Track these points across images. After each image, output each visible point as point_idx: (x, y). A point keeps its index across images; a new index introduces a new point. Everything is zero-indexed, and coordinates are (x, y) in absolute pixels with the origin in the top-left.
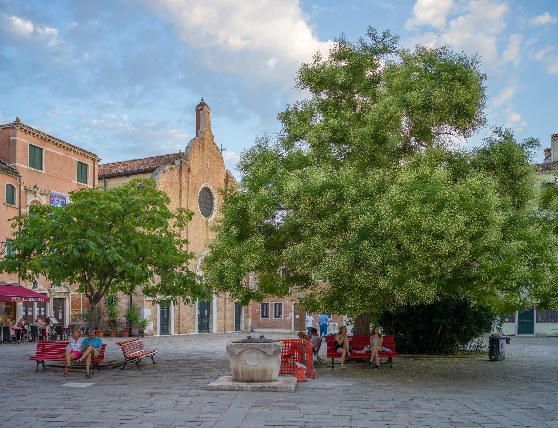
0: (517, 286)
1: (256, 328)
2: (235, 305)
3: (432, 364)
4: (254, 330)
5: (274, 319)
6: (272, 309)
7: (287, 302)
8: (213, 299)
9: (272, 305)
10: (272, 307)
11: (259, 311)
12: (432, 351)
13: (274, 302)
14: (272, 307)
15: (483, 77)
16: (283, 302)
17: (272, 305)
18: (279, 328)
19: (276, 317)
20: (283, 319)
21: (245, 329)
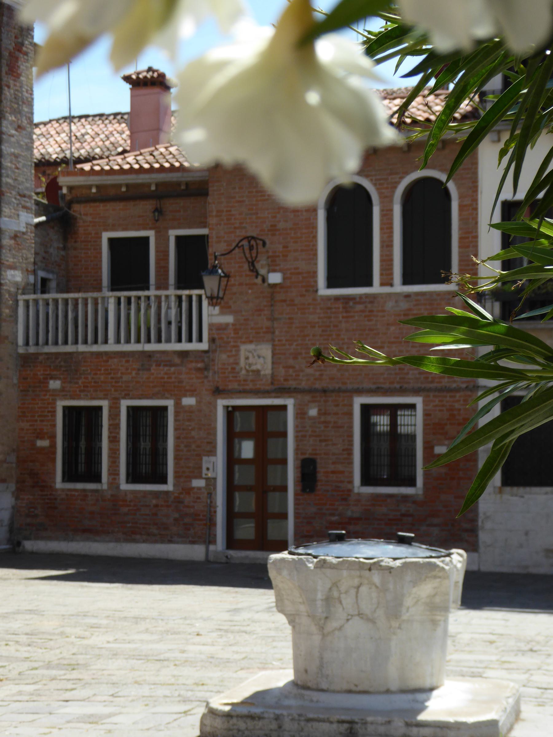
0: (45, 379)
4: (29, 545)
5: (125, 486)
6: (114, 439)
7: (189, 401)
8: (363, 388)
9: (114, 415)
10: (114, 427)
11: (53, 445)
12: (117, 477)
14: (114, 427)
15: (2, 259)
16: (170, 403)
17: (114, 415)
18: (151, 538)
20: (169, 487)
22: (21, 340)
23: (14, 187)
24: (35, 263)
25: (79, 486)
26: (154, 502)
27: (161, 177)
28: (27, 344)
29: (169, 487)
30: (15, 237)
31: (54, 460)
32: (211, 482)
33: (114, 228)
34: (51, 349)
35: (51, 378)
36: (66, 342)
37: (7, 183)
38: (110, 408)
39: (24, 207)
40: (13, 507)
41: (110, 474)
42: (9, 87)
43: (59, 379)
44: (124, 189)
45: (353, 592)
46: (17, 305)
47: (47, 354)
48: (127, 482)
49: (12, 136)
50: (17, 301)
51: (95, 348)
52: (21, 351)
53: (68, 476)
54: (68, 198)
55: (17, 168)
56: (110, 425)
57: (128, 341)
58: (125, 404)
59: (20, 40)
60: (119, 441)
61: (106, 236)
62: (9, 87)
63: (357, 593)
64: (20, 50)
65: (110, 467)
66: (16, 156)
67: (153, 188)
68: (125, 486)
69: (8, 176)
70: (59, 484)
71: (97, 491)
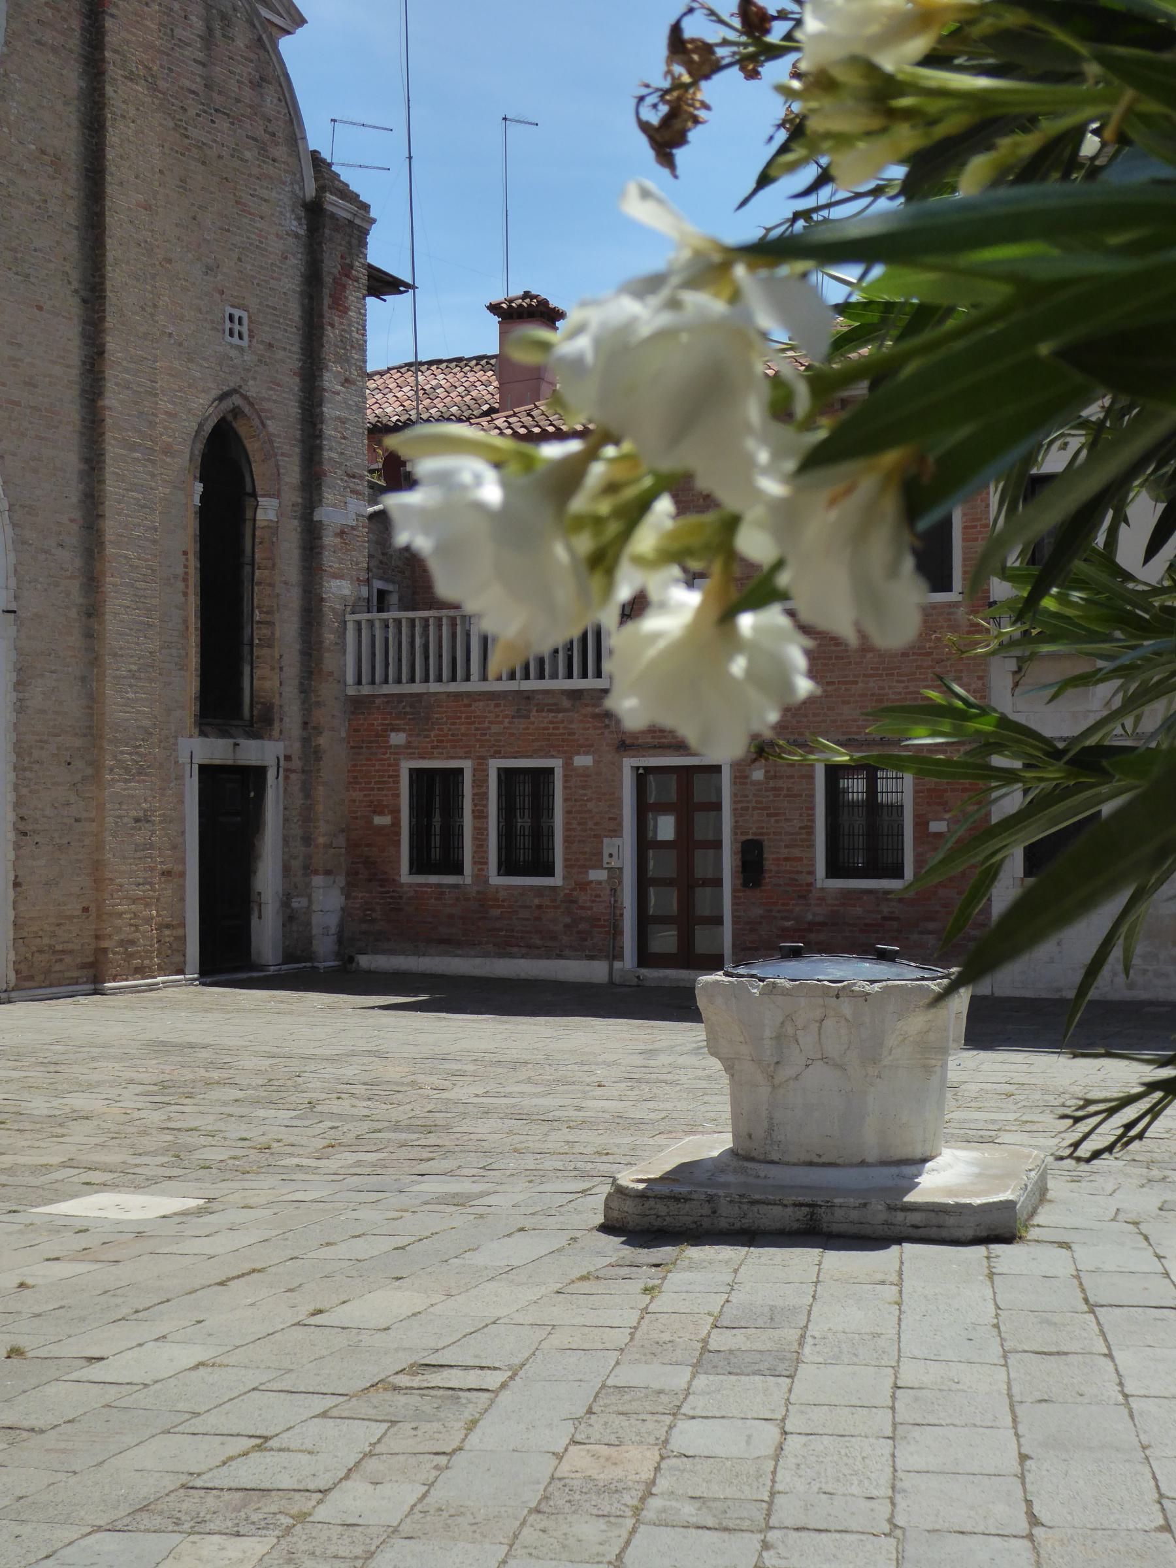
1: (376, 942)
2: (192, 788)
3: (1099, 1093)
4: (364, 961)
5: (496, 880)
6: (480, 815)
7: (583, 761)
9: (480, 781)
10: (481, 797)
11: (396, 823)
13: (494, 765)
14: (481, 797)
16: (556, 764)
17: (480, 781)
19: (508, 867)
20: (557, 880)
21: (289, 958)
22: (350, 678)
23: (341, 464)
25: (433, 879)
26: (537, 901)
29: (557, 880)
31: (397, 844)
32: (616, 874)
35: (392, 730)
37: (330, 459)
40: (342, 909)
42: (333, 326)
43: (404, 730)
46: (345, 629)
52: (351, 691)
53: (420, 865)
55: (344, 438)
58: (494, 765)
60: (486, 817)
62: (333, 326)
66: (343, 421)
69: (330, 449)
70: (405, 876)
71: (456, 886)
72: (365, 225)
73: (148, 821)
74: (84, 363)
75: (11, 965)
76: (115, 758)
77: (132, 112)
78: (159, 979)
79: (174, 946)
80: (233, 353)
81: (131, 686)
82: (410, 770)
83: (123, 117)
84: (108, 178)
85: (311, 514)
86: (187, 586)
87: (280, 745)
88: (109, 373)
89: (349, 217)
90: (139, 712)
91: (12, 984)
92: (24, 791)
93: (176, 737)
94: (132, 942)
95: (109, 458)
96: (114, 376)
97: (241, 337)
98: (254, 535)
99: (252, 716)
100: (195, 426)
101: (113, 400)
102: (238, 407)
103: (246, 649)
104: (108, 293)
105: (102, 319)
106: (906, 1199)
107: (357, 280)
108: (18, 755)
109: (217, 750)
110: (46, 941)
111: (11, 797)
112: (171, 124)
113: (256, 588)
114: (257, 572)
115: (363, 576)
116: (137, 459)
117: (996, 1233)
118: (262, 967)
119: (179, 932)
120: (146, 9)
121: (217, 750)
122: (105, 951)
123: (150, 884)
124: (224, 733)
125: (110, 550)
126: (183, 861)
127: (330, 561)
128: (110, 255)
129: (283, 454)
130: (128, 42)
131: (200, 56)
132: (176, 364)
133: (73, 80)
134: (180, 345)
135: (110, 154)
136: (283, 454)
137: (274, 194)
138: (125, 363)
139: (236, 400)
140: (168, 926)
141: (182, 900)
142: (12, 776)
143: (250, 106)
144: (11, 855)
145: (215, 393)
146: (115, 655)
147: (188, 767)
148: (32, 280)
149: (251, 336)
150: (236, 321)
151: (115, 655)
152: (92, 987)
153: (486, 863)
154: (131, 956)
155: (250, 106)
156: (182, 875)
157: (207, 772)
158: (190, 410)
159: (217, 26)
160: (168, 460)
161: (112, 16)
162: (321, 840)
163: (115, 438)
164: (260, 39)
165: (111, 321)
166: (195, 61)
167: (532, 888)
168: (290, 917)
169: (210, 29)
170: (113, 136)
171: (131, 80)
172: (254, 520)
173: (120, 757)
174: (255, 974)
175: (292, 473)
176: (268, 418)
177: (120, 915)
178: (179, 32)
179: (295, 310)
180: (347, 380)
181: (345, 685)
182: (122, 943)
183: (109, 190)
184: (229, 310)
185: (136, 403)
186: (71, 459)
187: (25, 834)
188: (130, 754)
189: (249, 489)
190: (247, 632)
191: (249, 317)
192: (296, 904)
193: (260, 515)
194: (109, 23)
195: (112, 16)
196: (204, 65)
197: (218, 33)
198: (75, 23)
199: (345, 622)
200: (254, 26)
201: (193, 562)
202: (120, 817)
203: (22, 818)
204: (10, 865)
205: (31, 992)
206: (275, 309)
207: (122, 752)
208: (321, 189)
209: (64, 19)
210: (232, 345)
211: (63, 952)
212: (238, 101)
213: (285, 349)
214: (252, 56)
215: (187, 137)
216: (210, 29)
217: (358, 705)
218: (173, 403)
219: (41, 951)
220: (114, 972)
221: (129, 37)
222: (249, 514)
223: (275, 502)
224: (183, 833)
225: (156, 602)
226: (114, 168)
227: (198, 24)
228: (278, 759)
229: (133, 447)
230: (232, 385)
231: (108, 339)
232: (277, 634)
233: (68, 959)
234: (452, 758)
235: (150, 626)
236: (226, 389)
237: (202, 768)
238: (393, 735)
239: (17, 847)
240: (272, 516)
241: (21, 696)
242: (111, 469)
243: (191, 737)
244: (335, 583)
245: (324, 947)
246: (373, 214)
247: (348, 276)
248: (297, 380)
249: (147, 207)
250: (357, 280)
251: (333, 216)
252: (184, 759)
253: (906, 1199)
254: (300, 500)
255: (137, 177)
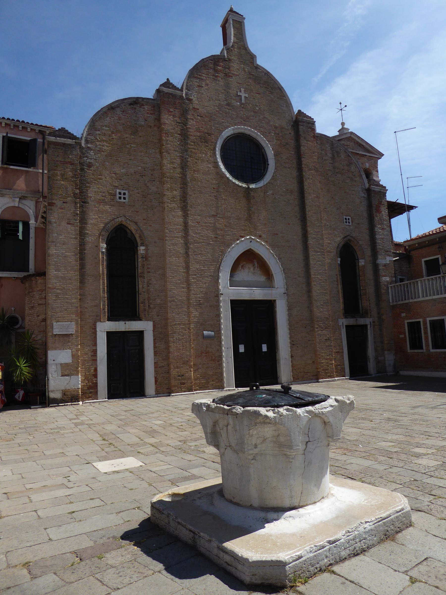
4: (402, 373)
5: (432, 351)
6: (426, 333)
11: (405, 336)
14: (426, 328)
22: (391, 301)
23: (383, 249)
24: (395, 274)
25: (416, 351)
26: (444, 356)
27: (439, 235)
28: (393, 302)
30: (385, 265)
31: (406, 342)
33: (426, 257)
34: (401, 302)
35: (402, 313)
36: (405, 300)
37: (379, 248)
38: (423, 321)
39: (388, 255)
40: (395, 359)
41: (426, 346)
42: (377, 216)
43: (405, 313)
44: (427, 243)
45: (225, 428)
46: (388, 289)
47: (400, 304)
48: (410, 349)
49: (380, 232)
50: (388, 287)
51: (415, 300)
52: (391, 304)
53: (412, 347)
54: (409, 250)
55: (384, 243)
56: (424, 328)
57: (427, 296)
58: (428, 319)
59: (380, 200)
60: (428, 334)
61: (423, 260)
62: (377, 216)
63: (227, 428)
64: (381, 204)
65: (426, 344)
66: (383, 238)
67: (438, 240)
68: (432, 351)
69: (379, 246)
70: (409, 351)
71: (422, 352)
72: (385, 191)
73: (329, 340)
74: (303, 235)
75: (292, 376)
76: (318, 325)
77: (311, 177)
78: (336, 378)
79: (342, 370)
80: (347, 227)
81: (321, 308)
82: (407, 322)
83: (309, 179)
84: (305, 193)
85: (376, 262)
86: (338, 283)
87: (371, 319)
88: (309, 236)
89: (379, 190)
90: (324, 314)
91: (292, 381)
92: (293, 335)
93: (338, 319)
94: (327, 370)
95: (310, 255)
96: (310, 237)
97: (349, 223)
98: (359, 269)
99: (362, 312)
100: (337, 245)
101: (311, 242)
102: (350, 239)
103: (359, 297)
104: (307, 218)
105: (306, 224)
106: (230, 545)
107: (384, 204)
108: (290, 326)
109: (351, 321)
110: (302, 370)
111: (289, 336)
112: (324, 178)
113: (361, 282)
114: (361, 278)
115: (393, 275)
116: (319, 255)
117: (270, 582)
118: (371, 375)
119: (342, 367)
120: (313, 154)
121: (351, 321)
122: (319, 372)
123: (331, 355)
124: (353, 317)
125: (312, 276)
126: (342, 349)
127: (382, 272)
128: (307, 210)
129: (365, 249)
130: (308, 162)
131: (331, 162)
132: (330, 231)
133: (295, 173)
134: (331, 227)
135: (305, 187)
136: (365, 249)
137: (356, 189)
138: (313, 233)
139: (349, 238)
140: (339, 365)
141: (343, 358)
142: (288, 331)
143: (347, 170)
144: (290, 350)
145: (342, 237)
146: (316, 301)
147: (342, 327)
148: (286, 218)
149: (352, 222)
150: (347, 219)
151: (316, 301)
152: (316, 381)
153: (429, 346)
154: (327, 373)
155: (347, 170)
156: (343, 352)
157: (348, 327)
158: (335, 242)
159: (335, 154)
160: (330, 254)
161: (304, 158)
162: (386, 342)
163: (312, 250)
164: (348, 155)
165: (308, 224)
166: (330, 163)
167: (442, 352)
168: (378, 362)
169: (333, 155)
170: (306, 183)
171: (310, 170)
172: (359, 265)
173: (319, 325)
174: (368, 377)
175: (368, 252)
176: (359, 241)
177: (323, 363)
178: (324, 158)
179: (365, 214)
180: (383, 229)
181: (390, 303)
182: (323, 370)
183: (306, 195)
184: (345, 217)
185: (317, 242)
186: (301, 257)
187: (294, 345)
188: (323, 324)
189: (357, 258)
190: (359, 292)
191: (351, 218)
192: (380, 358)
193: (360, 264)
194: (303, 159)
195: (304, 158)
196: (332, 164)
197: (336, 156)
198: (295, 161)
199: (388, 287)
200: (346, 152)
201: (339, 278)
202: (321, 339)
203: (293, 341)
204: (290, 352)
205: (298, 382)
206: (359, 215)
207: (320, 324)
208: (370, 185)
209: (291, 161)
210: (346, 225)
211: (307, 372)
212: (343, 170)
213: (363, 224)
214: (346, 159)
215: (329, 180)
216: (333, 155)
217: (393, 307)
218: (330, 241)
219: (300, 372)
220: (322, 377)
221: (309, 161)
222: (357, 264)
223: (363, 260)
224: (342, 342)
225: (327, 287)
226: (306, 190)
227: (330, 155)
228: (370, 322)
229: (317, 252)
230: (347, 234)
231: (308, 228)
232: (367, 292)
233: (308, 374)
234: (417, 319)
235: (327, 293)
236: (346, 235)
237: (346, 326)
238: (402, 314)
239: (291, 348)
240: (363, 264)
241: (290, 312)
242: (311, 258)
243: (342, 319)
244: (384, 278)
245: (390, 370)
246: (387, 189)
247: (381, 204)
248: (368, 231)
249: (317, 197)
250: (384, 204)
251: (374, 191)
252: (340, 324)
253: (230, 545)
254: (371, 259)
255: (314, 191)
